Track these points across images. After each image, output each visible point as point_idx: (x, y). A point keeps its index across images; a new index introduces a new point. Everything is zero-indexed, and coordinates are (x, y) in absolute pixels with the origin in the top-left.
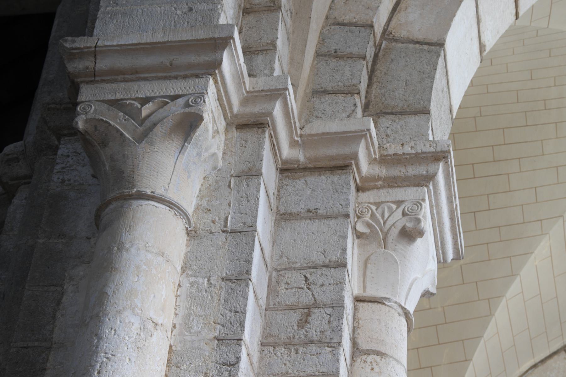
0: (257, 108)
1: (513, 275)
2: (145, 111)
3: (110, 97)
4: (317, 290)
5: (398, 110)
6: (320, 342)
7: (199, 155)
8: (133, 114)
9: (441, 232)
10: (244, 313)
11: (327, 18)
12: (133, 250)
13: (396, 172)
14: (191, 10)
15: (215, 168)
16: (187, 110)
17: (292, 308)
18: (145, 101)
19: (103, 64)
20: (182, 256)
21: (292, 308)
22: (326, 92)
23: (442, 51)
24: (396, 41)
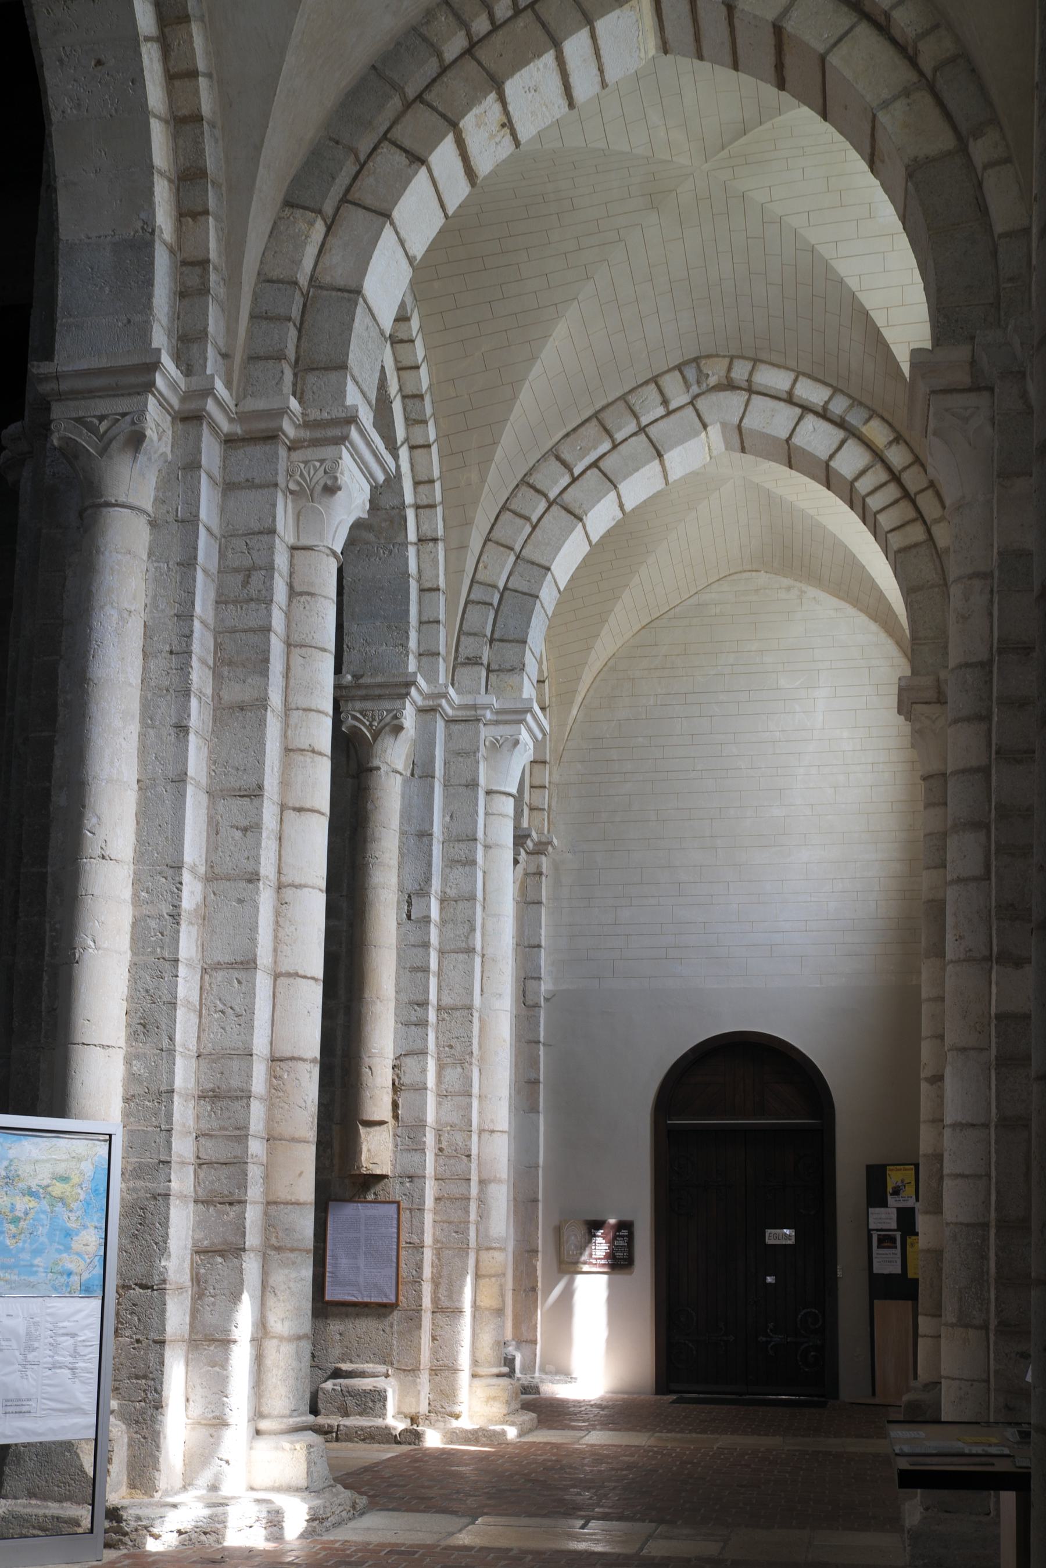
0: (192, 406)
1: (534, 358)
2: (102, 428)
3: (74, 415)
4: (254, 553)
5: (322, 365)
6: (258, 599)
7: (150, 459)
8: (93, 429)
9: (367, 468)
10: (194, 594)
11: (259, 274)
12: (107, 553)
13: (319, 434)
14: (129, 321)
15: (166, 461)
16: (133, 428)
17: (236, 570)
18: (102, 418)
19: (65, 386)
20: (147, 544)
21: (236, 570)
22: (258, 358)
23: (361, 299)
24: (321, 288)
